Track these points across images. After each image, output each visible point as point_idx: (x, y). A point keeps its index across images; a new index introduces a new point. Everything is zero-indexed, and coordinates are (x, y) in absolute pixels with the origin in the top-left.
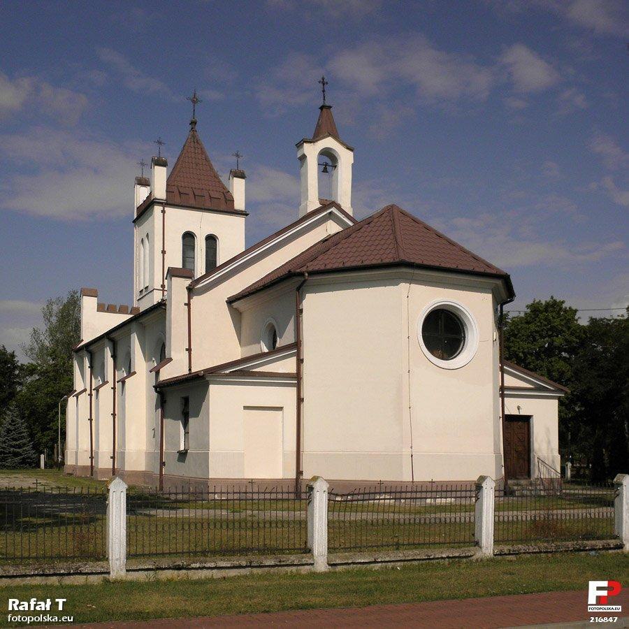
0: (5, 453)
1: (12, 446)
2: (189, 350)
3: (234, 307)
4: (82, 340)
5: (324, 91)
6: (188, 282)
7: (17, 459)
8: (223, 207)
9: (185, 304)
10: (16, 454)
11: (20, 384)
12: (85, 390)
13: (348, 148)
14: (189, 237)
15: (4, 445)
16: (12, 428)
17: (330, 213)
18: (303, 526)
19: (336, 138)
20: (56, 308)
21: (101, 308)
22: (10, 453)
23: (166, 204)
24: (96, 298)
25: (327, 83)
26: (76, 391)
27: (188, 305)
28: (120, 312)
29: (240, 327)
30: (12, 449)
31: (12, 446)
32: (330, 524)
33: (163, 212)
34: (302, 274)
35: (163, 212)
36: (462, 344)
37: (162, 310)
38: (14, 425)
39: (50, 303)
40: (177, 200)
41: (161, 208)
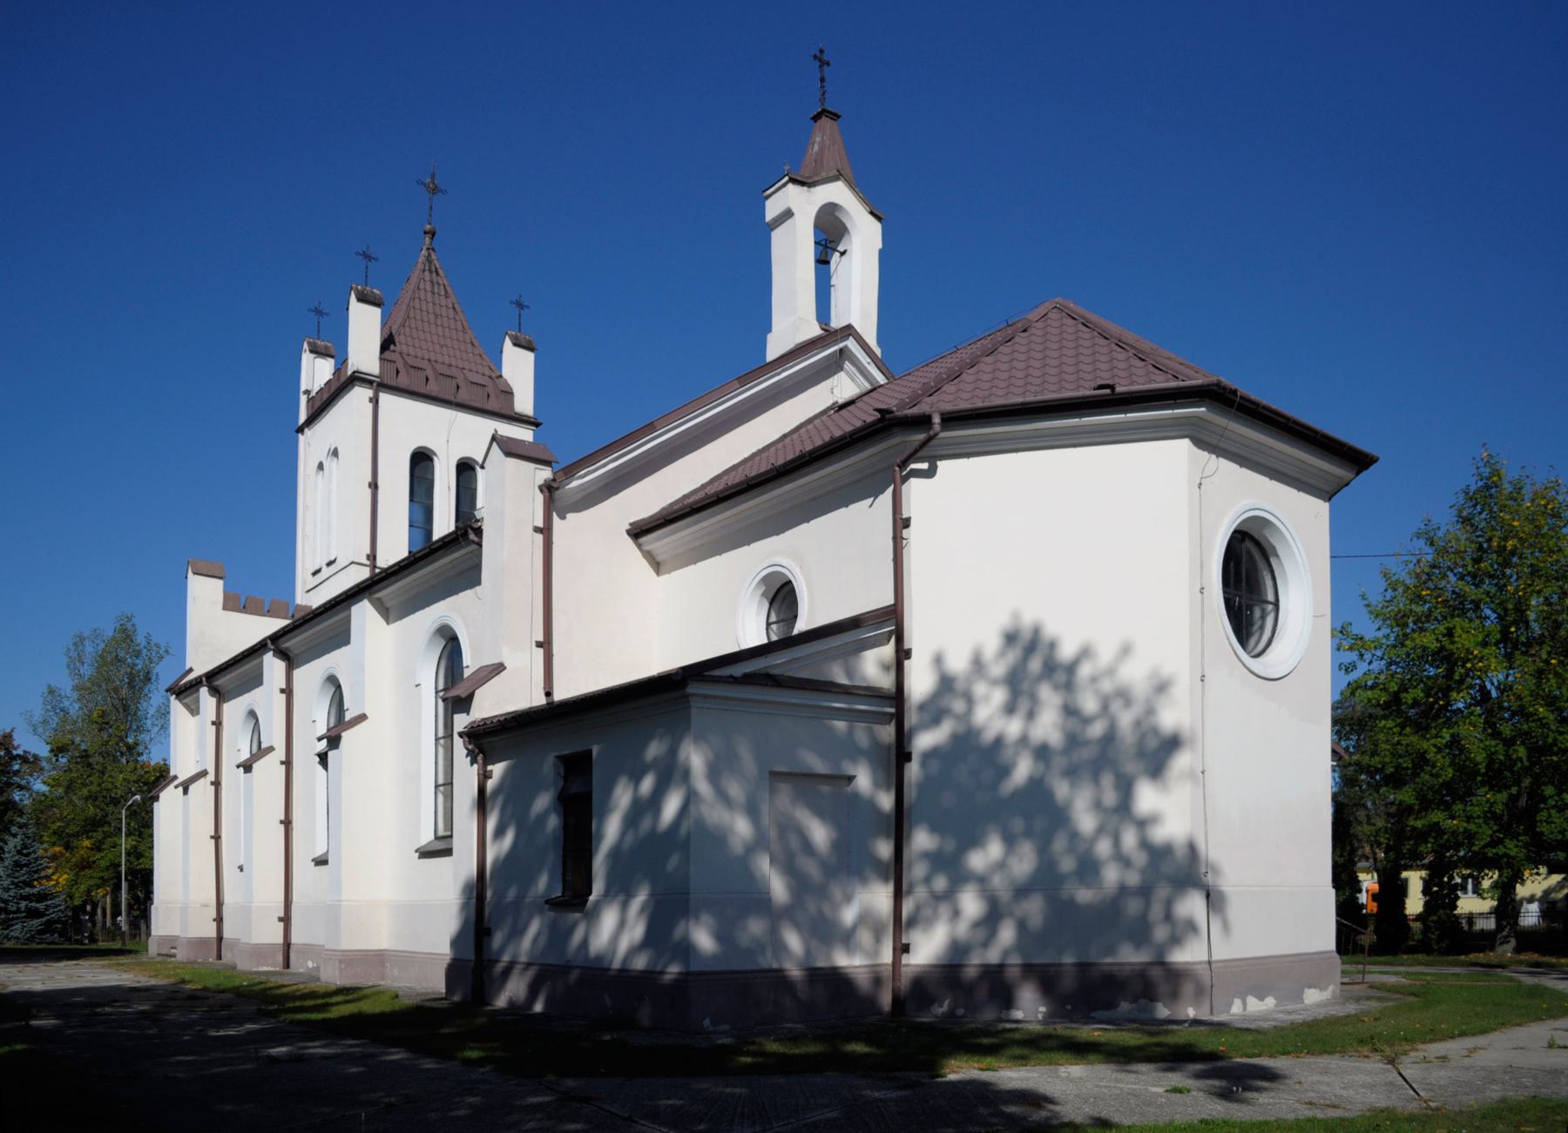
0: (7, 912)
1: (23, 898)
2: (546, 645)
3: (646, 548)
4: (191, 670)
5: (822, 80)
6: (545, 474)
7: (36, 923)
8: (492, 405)
9: (537, 530)
10: (33, 914)
11: (21, 788)
12: (204, 774)
13: (872, 213)
14: (421, 460)
15: (5, 896)
16: (24, 860)
17: (841, 350)
18: (121, 862)
19: (856, 186)
20: (89, 648)
21: (232, 603)
22: (18, 911)
23: (380, 385)
24: (220, 582)
25: (828, 64)
26: (175, 777)
27: (546, 531)
28: (270, 613)
29: (1172, 426)
30: (23, 904)
31: (23, 898)
32: (121, 858)
33: (375, 401)
34: (923, 421)
35: (375, 401)
36: (1269, 582)
37: (474, 547)
38: (28, 855)
39: (80, 641)
40: (403, 381)
41: (369, 393)
